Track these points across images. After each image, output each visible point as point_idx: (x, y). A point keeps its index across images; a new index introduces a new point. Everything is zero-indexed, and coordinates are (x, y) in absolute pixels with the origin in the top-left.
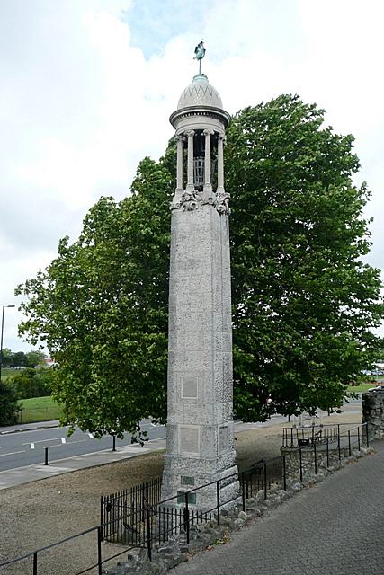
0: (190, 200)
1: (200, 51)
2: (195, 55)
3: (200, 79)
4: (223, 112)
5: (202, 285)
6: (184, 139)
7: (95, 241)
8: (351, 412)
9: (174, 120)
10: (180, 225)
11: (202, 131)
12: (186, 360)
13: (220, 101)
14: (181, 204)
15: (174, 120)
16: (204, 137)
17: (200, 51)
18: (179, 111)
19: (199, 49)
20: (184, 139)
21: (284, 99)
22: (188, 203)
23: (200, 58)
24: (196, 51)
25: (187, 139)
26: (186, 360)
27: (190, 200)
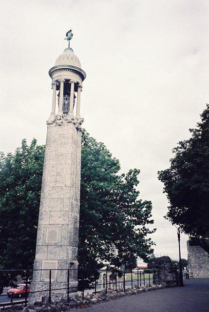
0: (60, 119)
1: (69, 36)
2: (66, 37)
3: (69, 51)
4: (80, 69)
5: (65, 170)
6: (58, 84)
7: (135, 220)
8: (5, 303)
9: (51, 74)
10: (53, 134)
11: (69, 80)
12: (51, 216)
13: (80, 65)
14: (54, 122)
15: (51, 74)
16: (70, 84)
17: (69, 36)
18: (53, 68)
19: (69, 34)
20: (58, 84)
21: (164, 257)
22: (59, 121)
23: (69, 39)
24: (67, 35)
25: (60, 84)
26: (51, 216)
27: (60, 119)
